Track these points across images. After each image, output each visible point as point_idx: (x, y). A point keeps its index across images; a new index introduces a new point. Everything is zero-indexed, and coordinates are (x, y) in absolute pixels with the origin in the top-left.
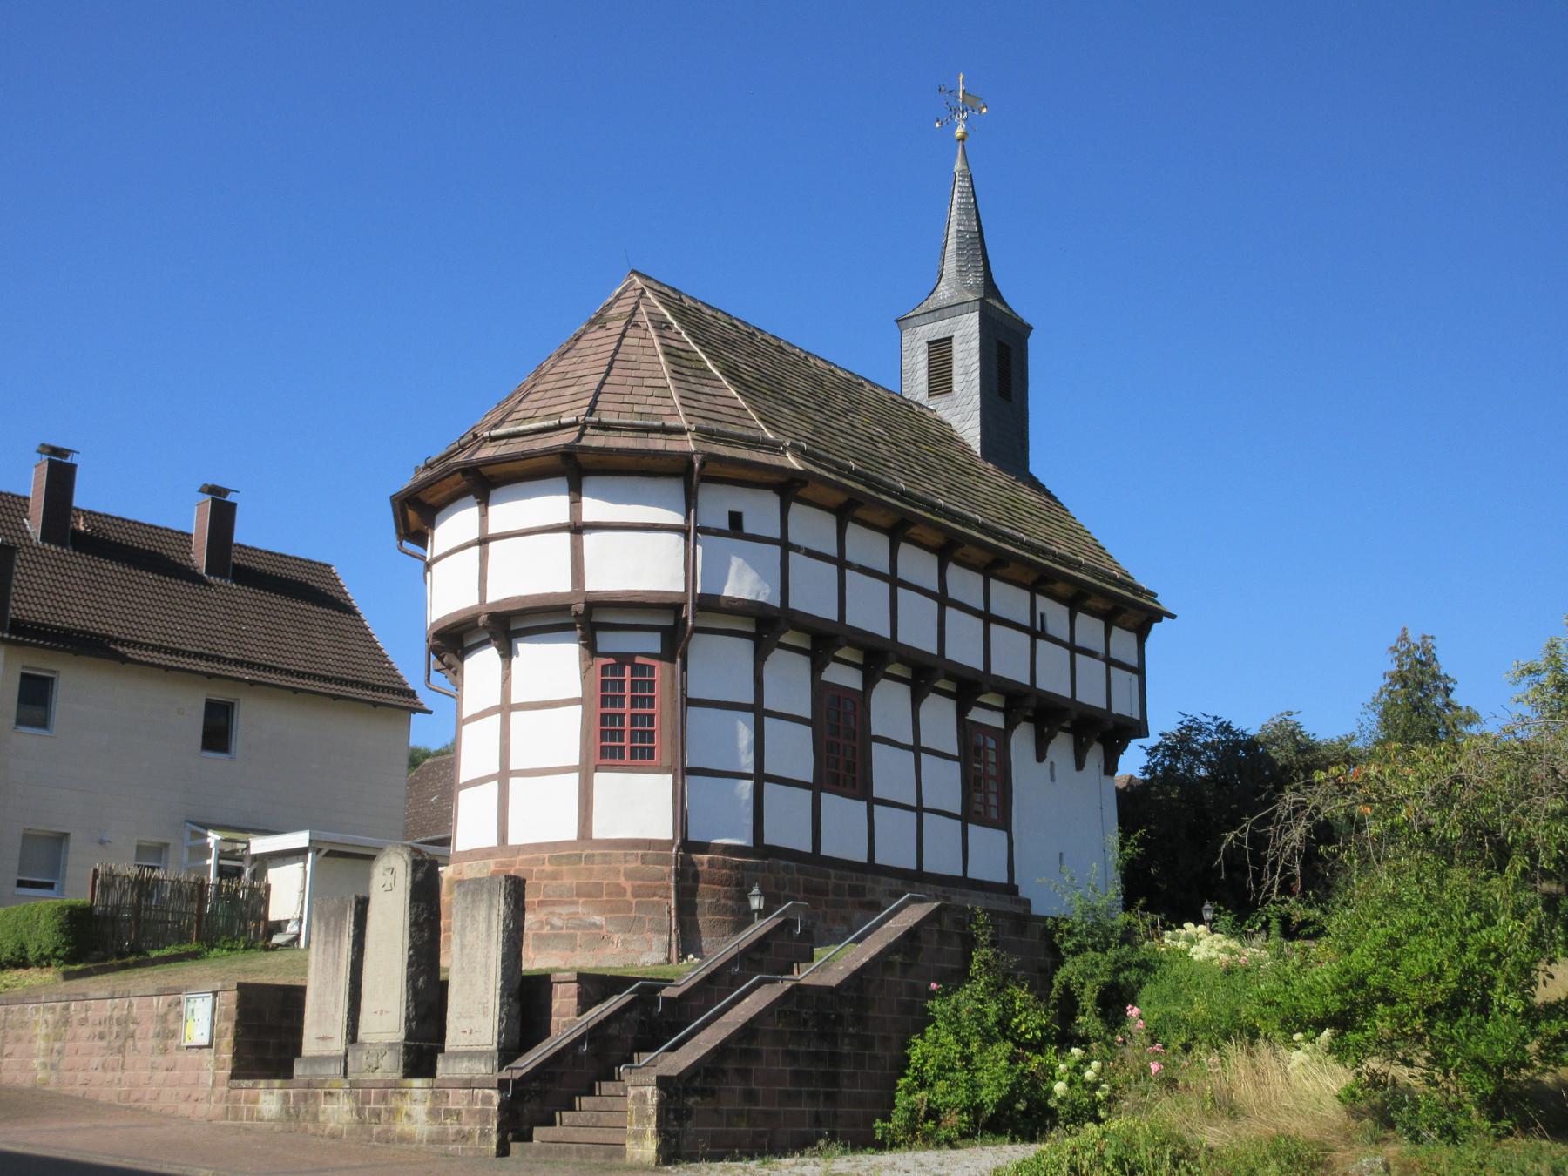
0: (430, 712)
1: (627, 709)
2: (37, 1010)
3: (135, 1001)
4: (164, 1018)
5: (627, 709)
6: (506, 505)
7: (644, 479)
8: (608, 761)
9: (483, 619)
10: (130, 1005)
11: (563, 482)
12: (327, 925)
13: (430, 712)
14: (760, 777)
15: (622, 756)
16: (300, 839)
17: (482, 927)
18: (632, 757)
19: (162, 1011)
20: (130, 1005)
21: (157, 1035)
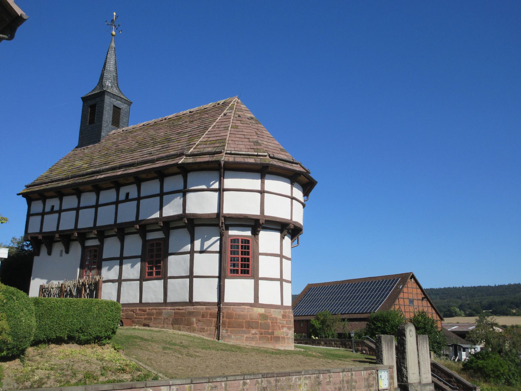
0: (18, 194)
1: (240, 256)
2: (300, 379)
3: (354, 373)
4: (367, 379)
5: (240, 256)
6: (282, 182)
7: (211, 172)
8: (243, 275)
9: (292, 227)
10: (352, 375)
11: (259, 175)
12: (388, 344)
13: (18, 194)
14: (191, 276)
15: (238, 273)
16: (95, 266)
17: (425, 348)
18: (241, 273)
19: (366, 377)
20: (352, 375)
21: (365, 387)
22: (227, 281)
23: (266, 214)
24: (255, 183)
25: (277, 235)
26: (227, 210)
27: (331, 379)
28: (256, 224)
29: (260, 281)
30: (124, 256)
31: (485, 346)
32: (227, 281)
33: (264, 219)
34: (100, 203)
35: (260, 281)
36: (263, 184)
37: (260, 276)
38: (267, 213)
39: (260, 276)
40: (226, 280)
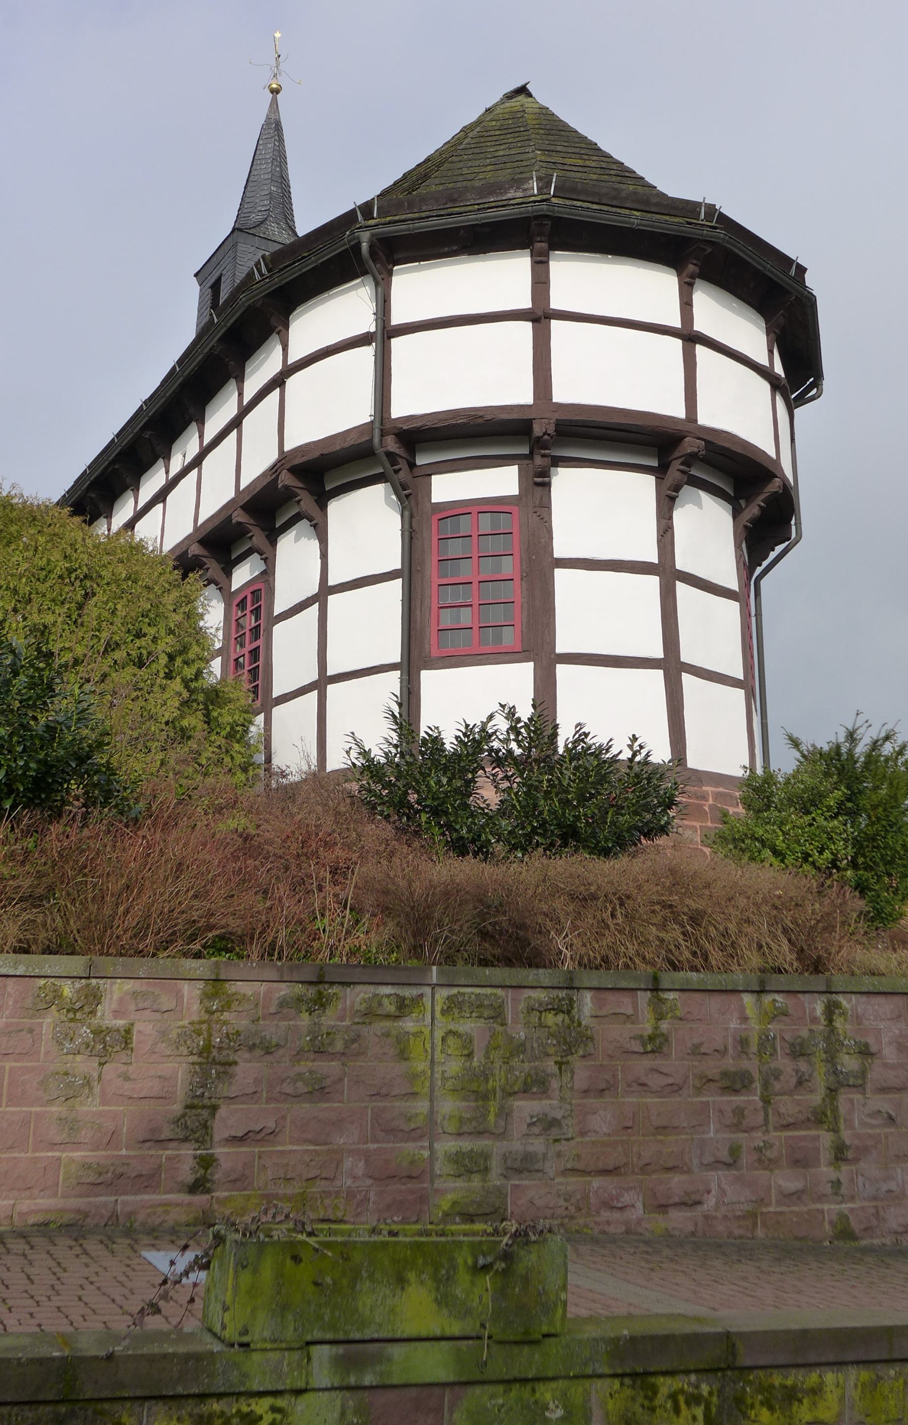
10: (831, 1009)
22: (425, 675)
23: (560, 395)
24: (504, 278)
25: (640, 489)
26: (567, 391)
27: (664, 1026)
28: (549, 437)
29: (562, 670)
30: (330, 673)
31: (854, 768)
32: (425, 675)
33: (557, 416)
34: (367, 354)
35: (562, 670)
36: (541, 283)
37: (560, 649)
38: (560, 395)
39: (560, 649)
40: (424, 673)
